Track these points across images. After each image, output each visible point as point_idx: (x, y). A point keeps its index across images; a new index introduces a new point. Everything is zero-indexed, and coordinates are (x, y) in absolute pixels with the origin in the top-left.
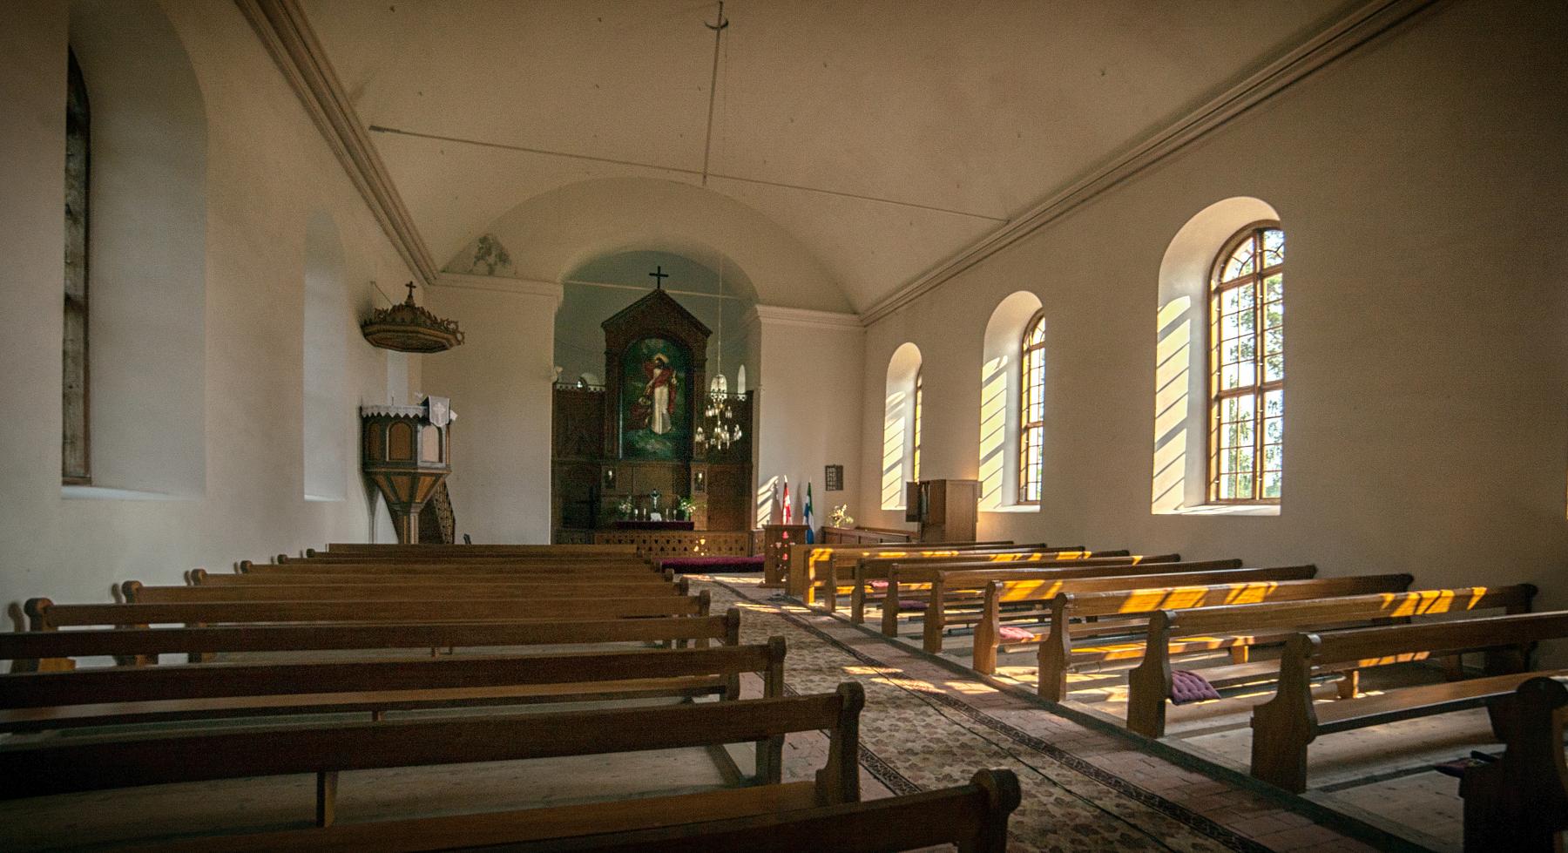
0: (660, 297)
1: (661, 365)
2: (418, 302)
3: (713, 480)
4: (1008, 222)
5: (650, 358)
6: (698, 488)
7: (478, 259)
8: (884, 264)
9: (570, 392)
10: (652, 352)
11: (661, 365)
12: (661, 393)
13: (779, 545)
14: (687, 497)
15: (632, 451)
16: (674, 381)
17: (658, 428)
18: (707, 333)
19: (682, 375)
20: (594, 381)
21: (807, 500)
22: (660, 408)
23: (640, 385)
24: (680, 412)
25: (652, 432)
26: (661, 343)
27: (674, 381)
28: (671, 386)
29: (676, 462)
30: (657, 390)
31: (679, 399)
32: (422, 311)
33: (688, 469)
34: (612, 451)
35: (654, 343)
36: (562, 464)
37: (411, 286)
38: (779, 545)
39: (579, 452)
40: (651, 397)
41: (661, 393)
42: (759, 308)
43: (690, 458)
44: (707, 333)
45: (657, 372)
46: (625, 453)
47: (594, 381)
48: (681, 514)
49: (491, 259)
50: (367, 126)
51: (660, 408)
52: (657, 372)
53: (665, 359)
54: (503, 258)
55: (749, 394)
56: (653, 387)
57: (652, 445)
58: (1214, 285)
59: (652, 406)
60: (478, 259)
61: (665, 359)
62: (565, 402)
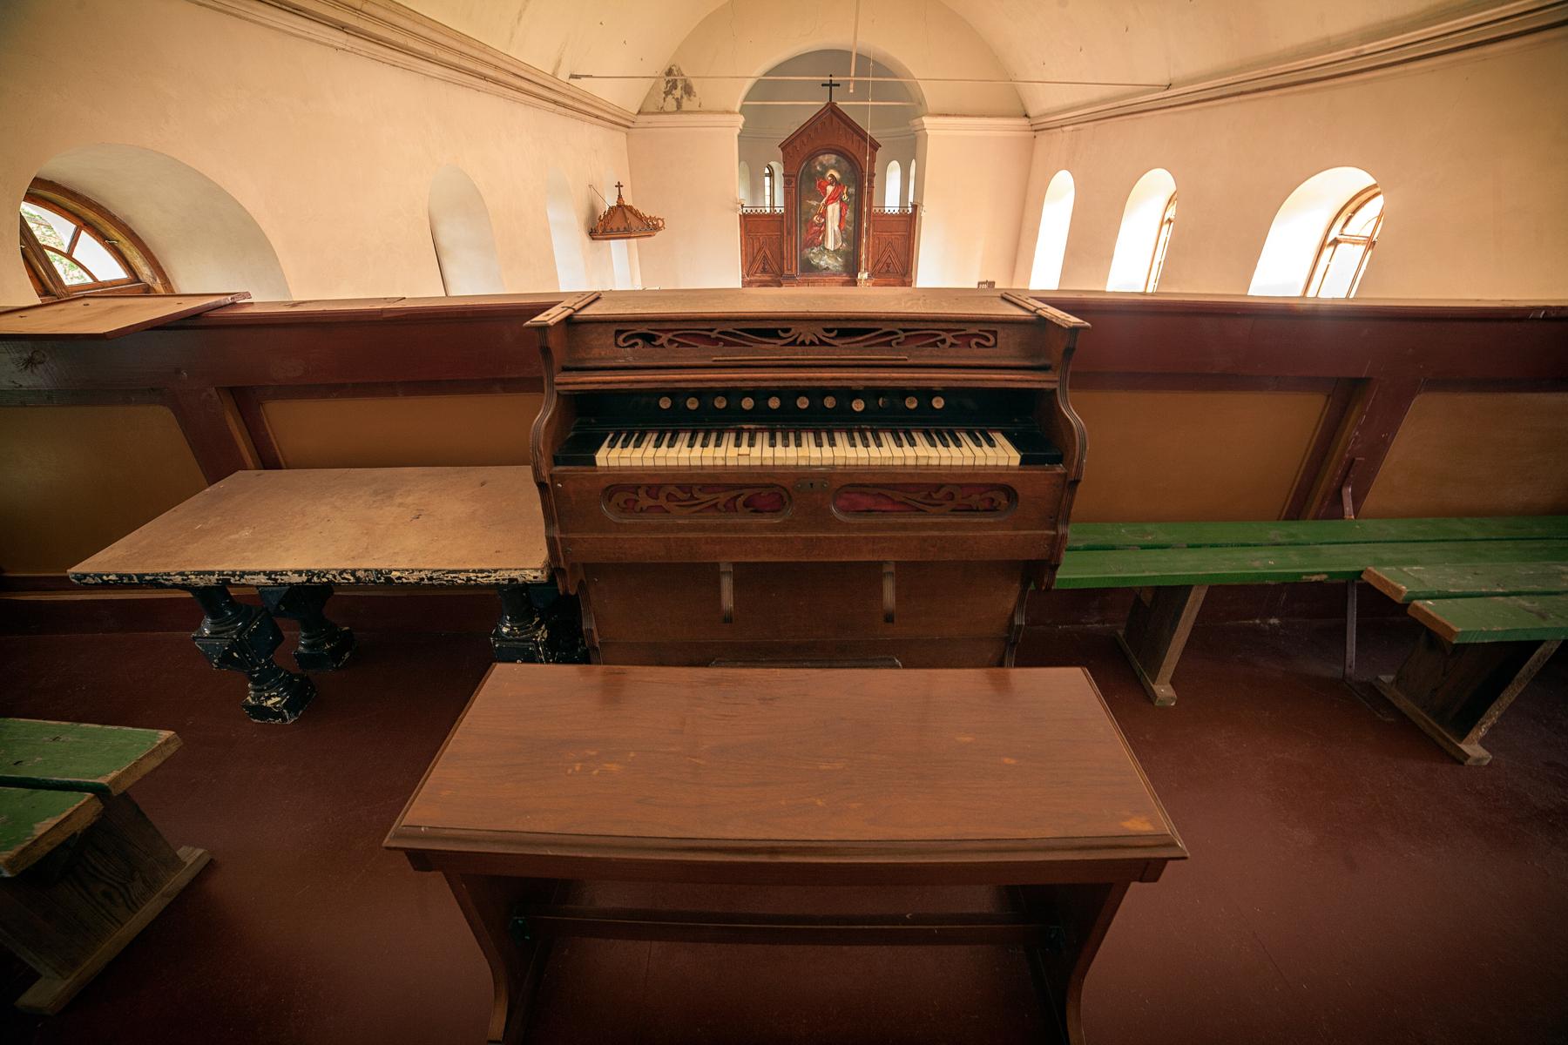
0: (832, 109)
1: (834, 181)
2: (628, 202)
4: (1169, 87)
5: (823, 174)
7: (667, 93)
8: (1061, 75)
9: (758, 216)
10: (826, 169)
12: (833, 210)
16: (845, 198)
17: (830, 245)
18: (875, 146)
19: (852, 190)
20: (773, 197)
22: (833, 225)
27: (845, 198)
30: (830, 208)
31: (849, 215)
32: (630, 209)
35: (829, 159)
37: (619, 186)
39: (764, 271)
40: (824, 215)
41: (833, 210)
42: (926, 120)
44: (875, 146)
47: (773, 197)
49: (678, 93)
50: (566, 79)
51: (833, 225)
52: (830, 189)
53: (837, 175)
55: (915, 207)
57: (826, 261)
58: (1334, 234)
59: (825, 224)
60: (667, 93)
61: (837, 175)
62: (751, 223)
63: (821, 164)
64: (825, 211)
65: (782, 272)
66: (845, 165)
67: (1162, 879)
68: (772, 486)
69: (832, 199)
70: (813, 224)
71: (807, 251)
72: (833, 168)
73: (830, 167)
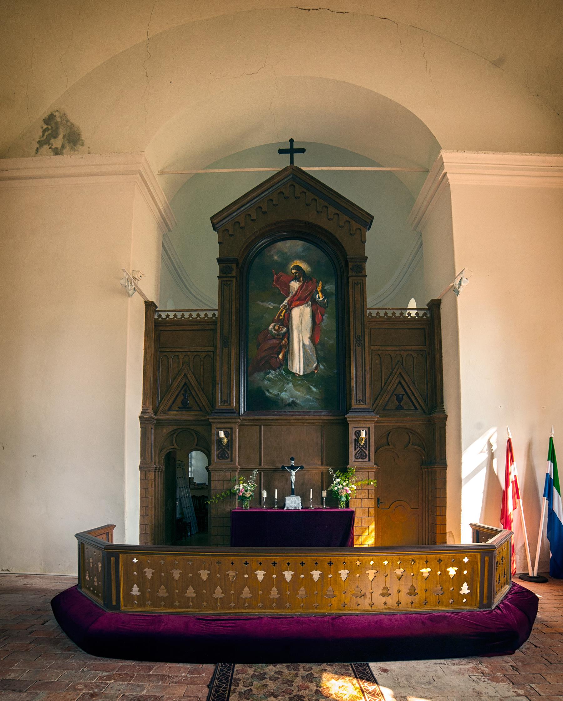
1: (300, 275)
3: (384, 442)
5: (283, 267)
6: (361, 456)
10: (287, 259)
11: (300, 275)
12: (301, 316)
13: (452, 571)
14: (343, 468)
15: (259, 401)
16: (320, 297)
17: (298, 366)
19: (331, 287)
21: (548, 468)
23: (271, 306)
24: (331, 341)
25: (289, 372)
26: (297, 246)
28: (314, 302)
29: (325, 416)
30: (296, 312)
31: (328, 322)
33: (345, 425)
34: (228, 401)
36: (159, 424)
38: (452, 571)
39: (185, 407)
40: (286, 321)
41: (301, 316)
43: (347, 409)
45: (295, 285)
46: (249, 407)
48: (334, 497)
49: (57, 143)
50: (370, 608)
52: (295, 285)
53: (304, 266)
54: (74, 139)
56: (289, 309)
57: (289, 393)
59: (288, 335)
62: (162, 332)
63: (281, 253)
64: (289, 316)
65: (212, 403)
66: (317, 253)
67: (138, 419)
68: (90, 600)
69: (299, 300)
70: (268, 335)
71: (257, 376)
72: (300, 258)
73: (295, 256)
